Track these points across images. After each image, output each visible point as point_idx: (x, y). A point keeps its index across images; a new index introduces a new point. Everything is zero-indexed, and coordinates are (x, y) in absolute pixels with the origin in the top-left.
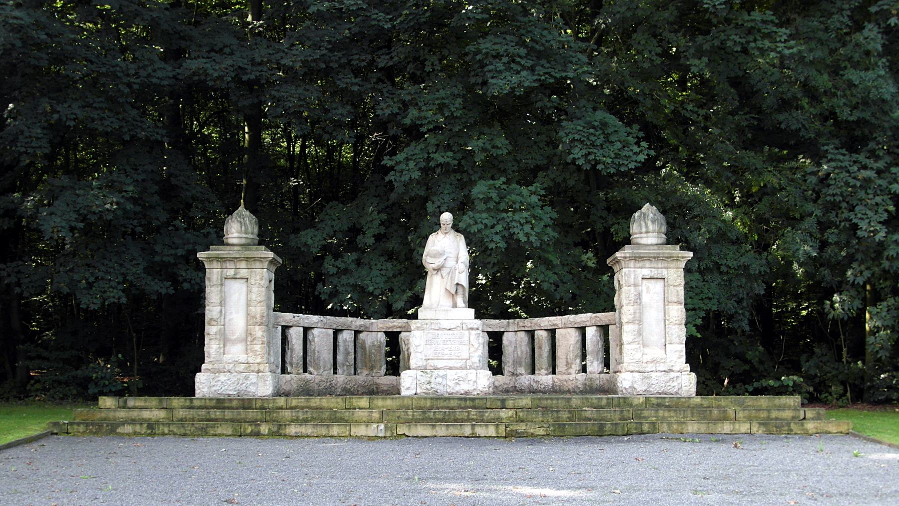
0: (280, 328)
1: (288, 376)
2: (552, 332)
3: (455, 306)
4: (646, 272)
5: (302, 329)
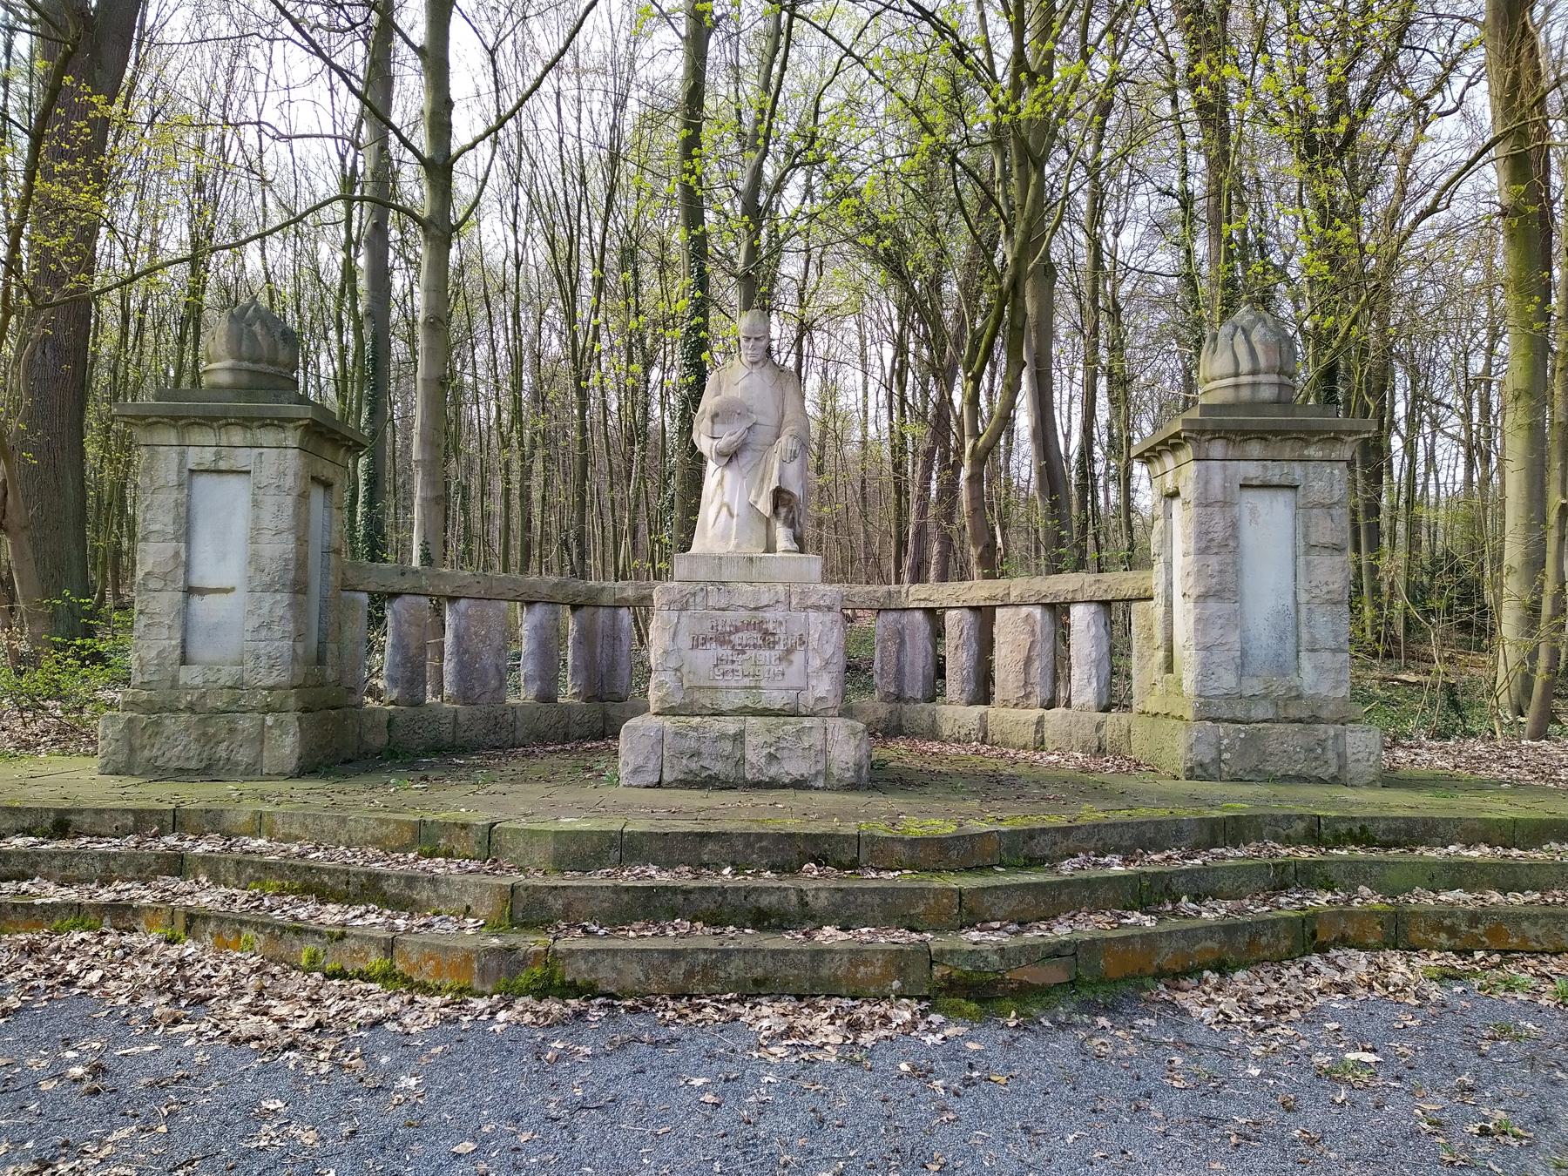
4: (1252, 470)
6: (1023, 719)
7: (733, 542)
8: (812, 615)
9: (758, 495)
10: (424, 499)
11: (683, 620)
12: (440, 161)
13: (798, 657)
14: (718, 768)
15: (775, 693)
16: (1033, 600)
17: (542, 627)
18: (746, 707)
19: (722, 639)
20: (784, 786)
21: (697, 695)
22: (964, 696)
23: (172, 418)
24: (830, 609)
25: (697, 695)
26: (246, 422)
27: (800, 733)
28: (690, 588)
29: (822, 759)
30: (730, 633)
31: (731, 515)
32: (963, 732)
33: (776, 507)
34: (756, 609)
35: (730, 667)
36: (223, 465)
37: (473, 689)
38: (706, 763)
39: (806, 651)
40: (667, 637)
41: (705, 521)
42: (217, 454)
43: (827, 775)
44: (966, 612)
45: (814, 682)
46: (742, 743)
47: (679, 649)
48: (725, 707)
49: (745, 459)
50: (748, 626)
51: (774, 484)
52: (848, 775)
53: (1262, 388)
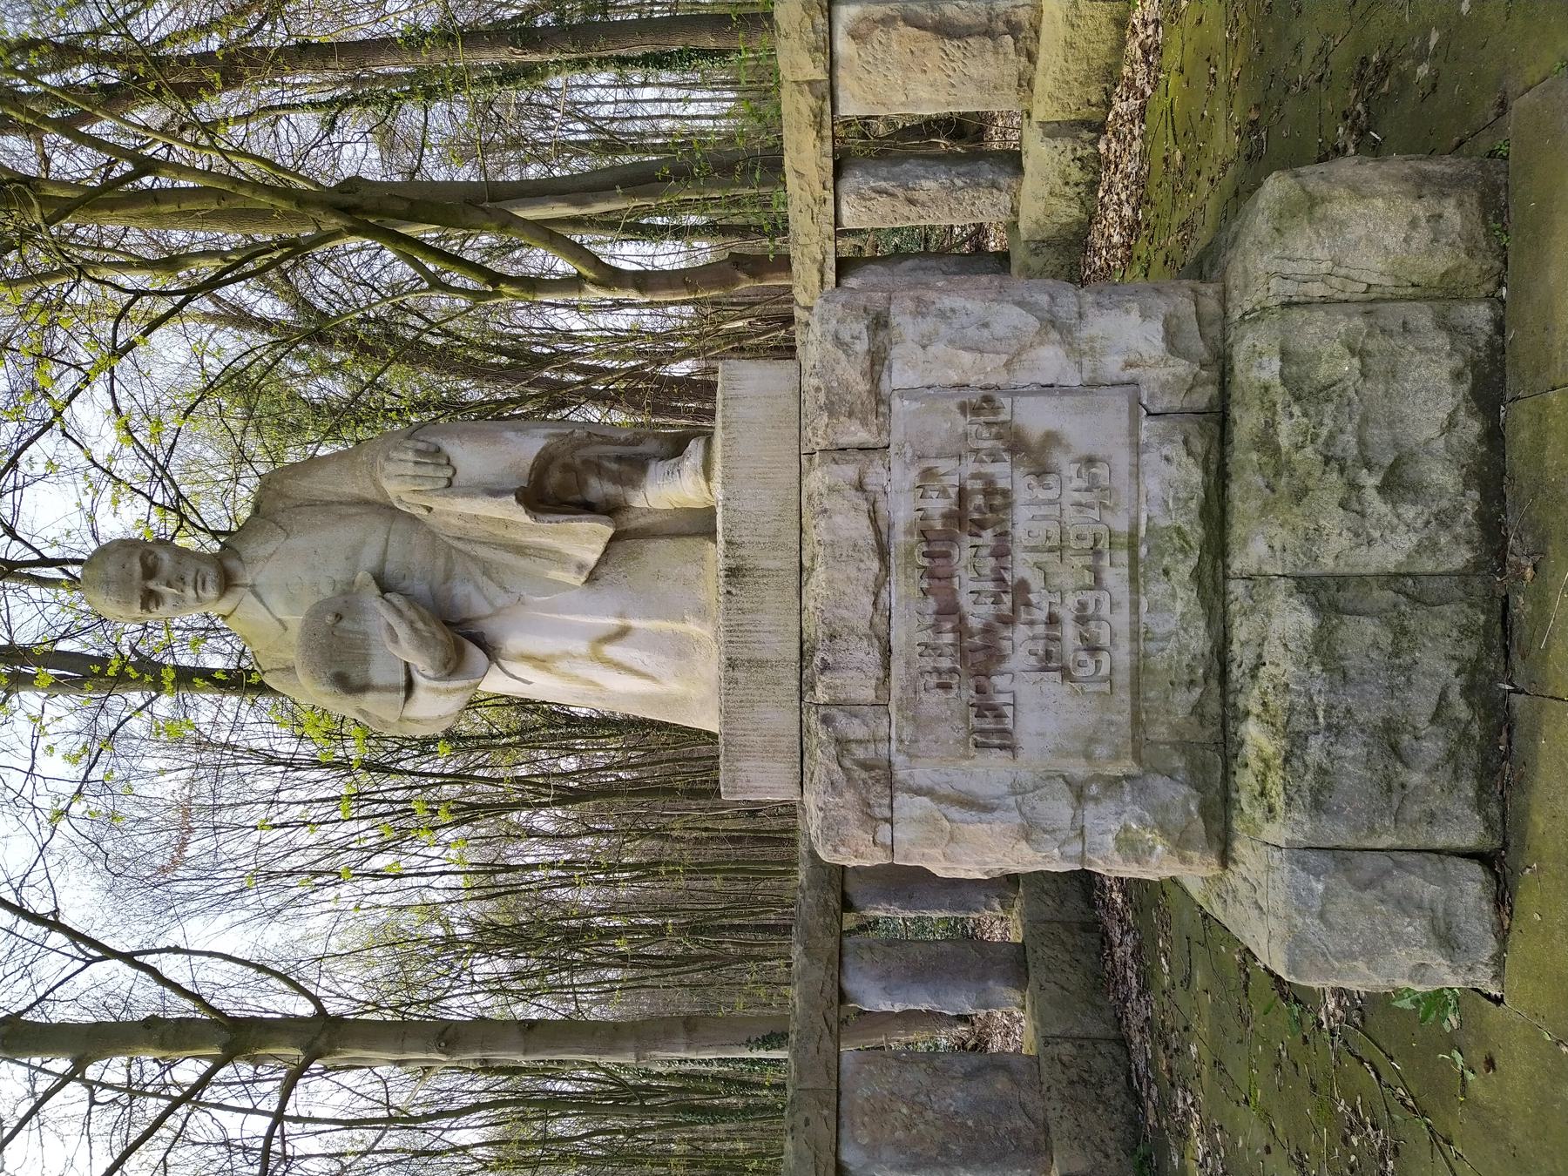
6: (1063, 31)
7: (693, 627)
8: (900, 376)
9: (560, 559)
10: (689, 1047)
11: (923, 774)
12: (225, 1036)
13: (1035, 417)
14: (1438, 663)
15: (1152, 485)
16: (821, 21)
17: (886, 976)
18: (1197, 575)
19: (980, 657)
20: (1495, 436)
21: (1160, 732)
22: (1004, 181)
24: (880, 323)
25: (1160, 732)
27: (1303, 390)
28: (822, 760)
29: (1392, 315)
30: (961, 630)
31: (622, 633)
32: (1076, 174)
33: (587, 508)
34: (883, 552)
35: (1070, 632)
37: (1015, 1132)
38: (1422, 705)
39: (1014, 392)
40: (977, 828)
41: (644, 699)
43: (1443, 294)
44: (848, 183)
45: (1113, 366)
46: (1342, 581)
47: (1016, 789)
48: (1199, 641)
49: (473, 597)
50: (937, 576)
51: (509, 510)
52: (1453, 215)
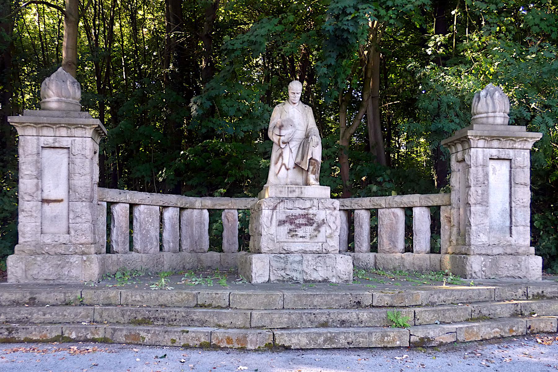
0: (105, 204)
1: (114, 256)
2: (374, 213)
3: (307, 183)
4: (494, 152)
5: (128, 206)
23: (35, 124)
26: (68, 126)
35: (294, 233)
36: (57, 145)
37: (147, 246)
38: (288, 273)
42: (54, 140)
53: (497, 118)
